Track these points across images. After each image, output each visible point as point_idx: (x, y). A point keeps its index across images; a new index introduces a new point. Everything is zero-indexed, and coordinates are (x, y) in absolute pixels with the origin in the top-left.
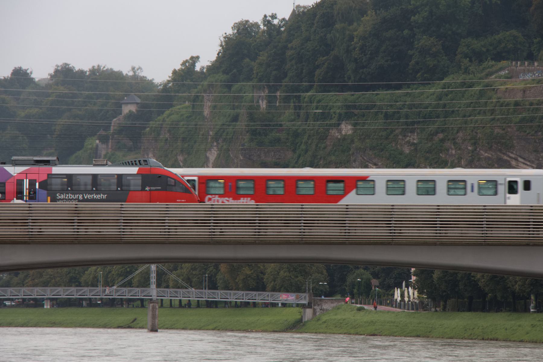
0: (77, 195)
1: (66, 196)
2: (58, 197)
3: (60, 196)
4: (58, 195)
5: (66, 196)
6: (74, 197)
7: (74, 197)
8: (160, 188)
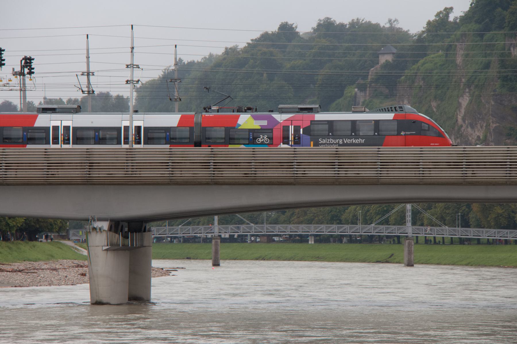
0: (338, 140)
1: (327, 141)
2: (321, 142)
3: (322, 141)
4: (320, 140)
5: (327, 141)
6: (335, 142)
7: (335, 142)
8: (415, 132)
